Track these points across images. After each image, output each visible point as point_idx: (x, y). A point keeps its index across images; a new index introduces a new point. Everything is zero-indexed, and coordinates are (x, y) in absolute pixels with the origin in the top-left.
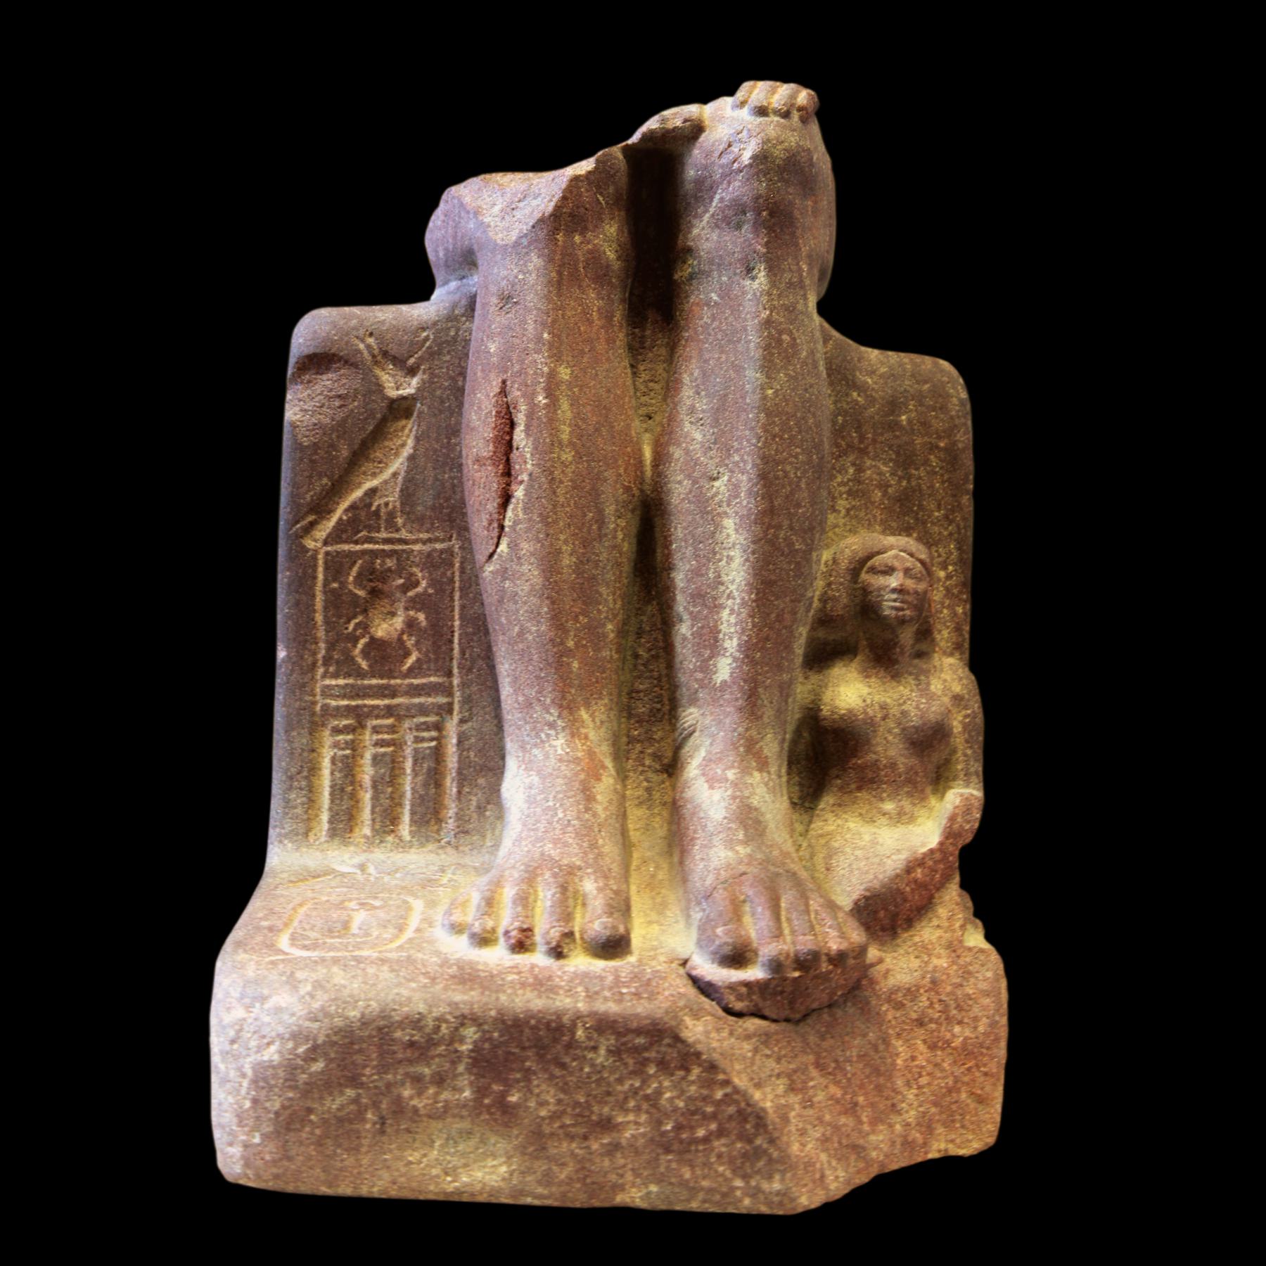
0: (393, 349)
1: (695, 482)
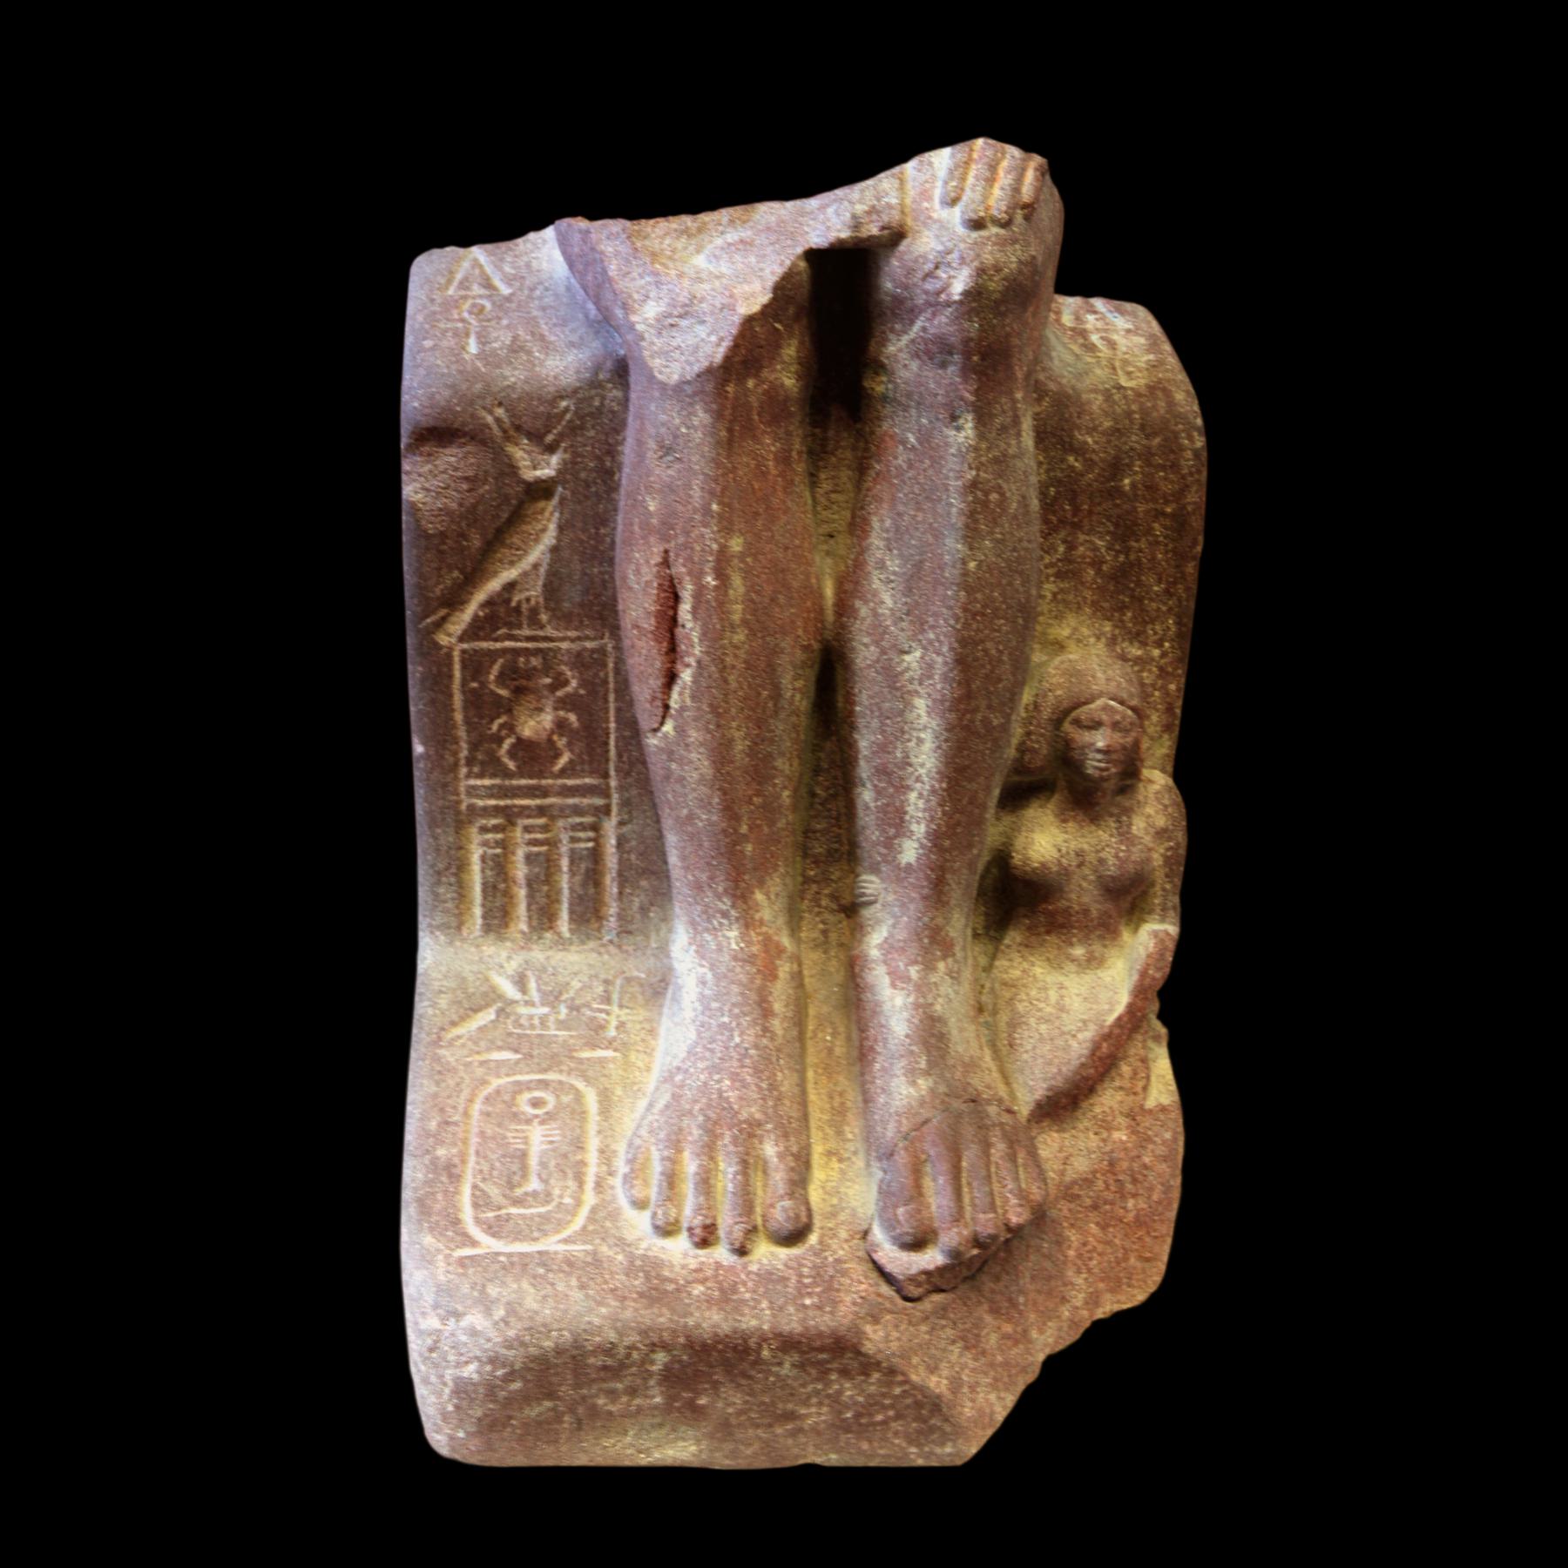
0: (527, 422)
1: (883, 652)
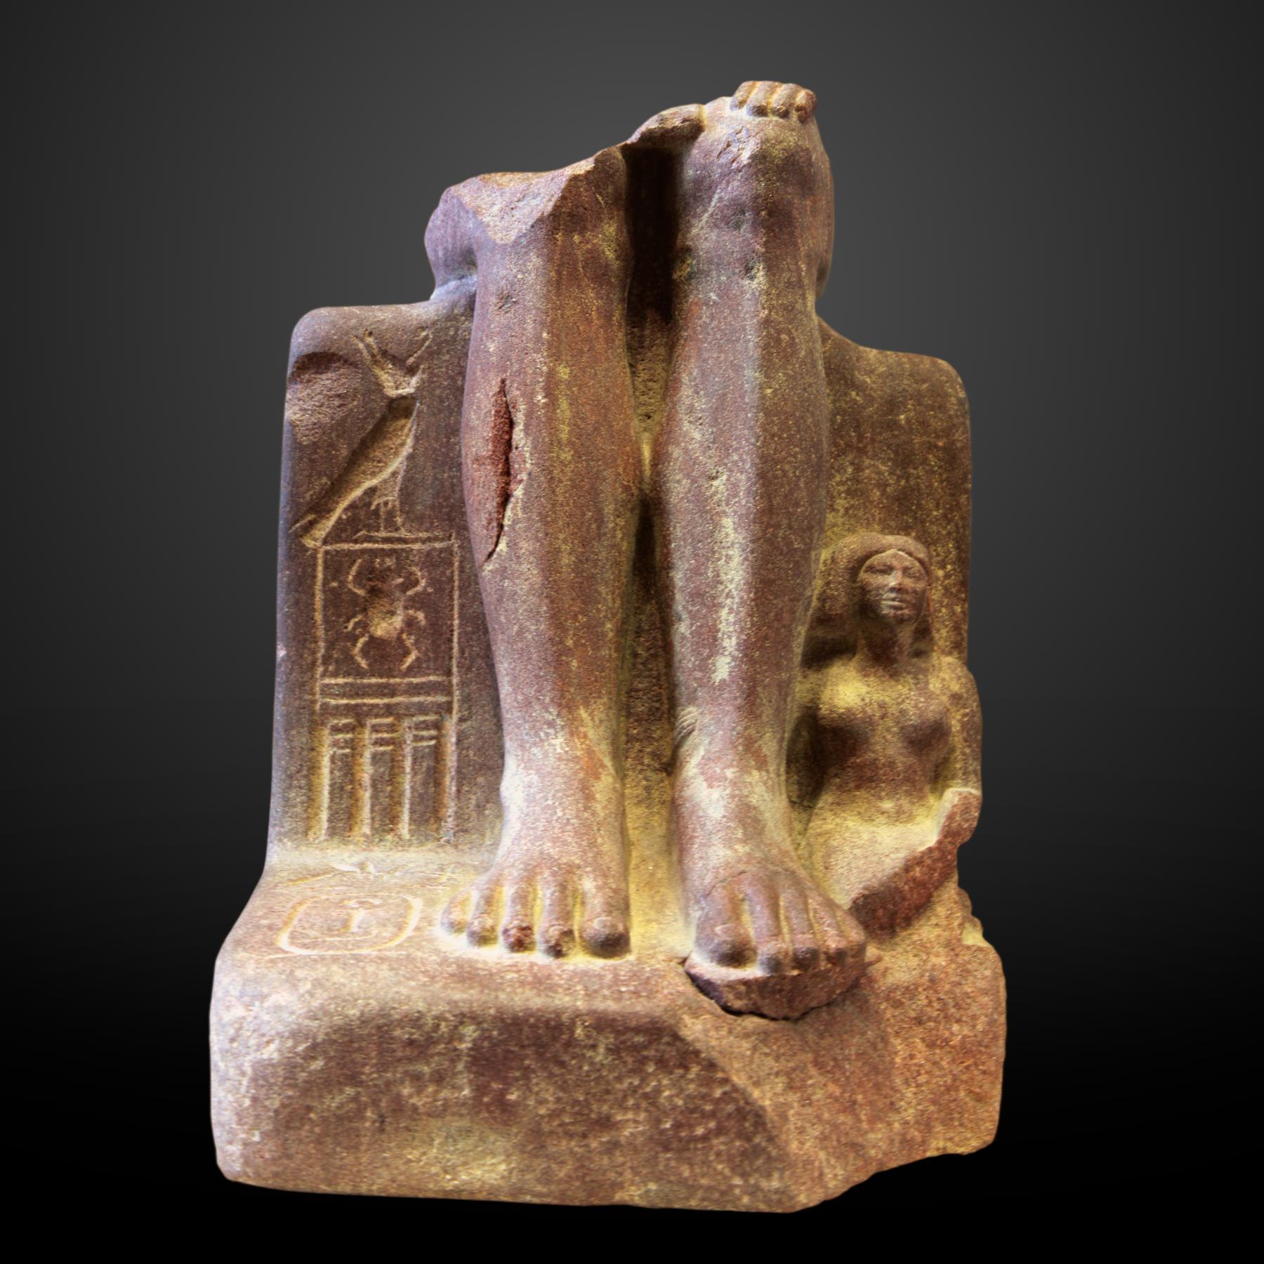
0: (393, 349)
1: (694, 481)
